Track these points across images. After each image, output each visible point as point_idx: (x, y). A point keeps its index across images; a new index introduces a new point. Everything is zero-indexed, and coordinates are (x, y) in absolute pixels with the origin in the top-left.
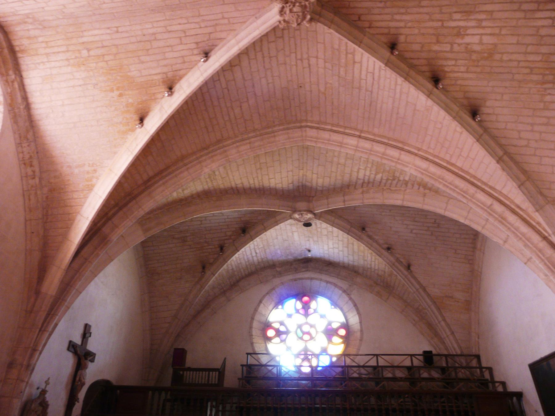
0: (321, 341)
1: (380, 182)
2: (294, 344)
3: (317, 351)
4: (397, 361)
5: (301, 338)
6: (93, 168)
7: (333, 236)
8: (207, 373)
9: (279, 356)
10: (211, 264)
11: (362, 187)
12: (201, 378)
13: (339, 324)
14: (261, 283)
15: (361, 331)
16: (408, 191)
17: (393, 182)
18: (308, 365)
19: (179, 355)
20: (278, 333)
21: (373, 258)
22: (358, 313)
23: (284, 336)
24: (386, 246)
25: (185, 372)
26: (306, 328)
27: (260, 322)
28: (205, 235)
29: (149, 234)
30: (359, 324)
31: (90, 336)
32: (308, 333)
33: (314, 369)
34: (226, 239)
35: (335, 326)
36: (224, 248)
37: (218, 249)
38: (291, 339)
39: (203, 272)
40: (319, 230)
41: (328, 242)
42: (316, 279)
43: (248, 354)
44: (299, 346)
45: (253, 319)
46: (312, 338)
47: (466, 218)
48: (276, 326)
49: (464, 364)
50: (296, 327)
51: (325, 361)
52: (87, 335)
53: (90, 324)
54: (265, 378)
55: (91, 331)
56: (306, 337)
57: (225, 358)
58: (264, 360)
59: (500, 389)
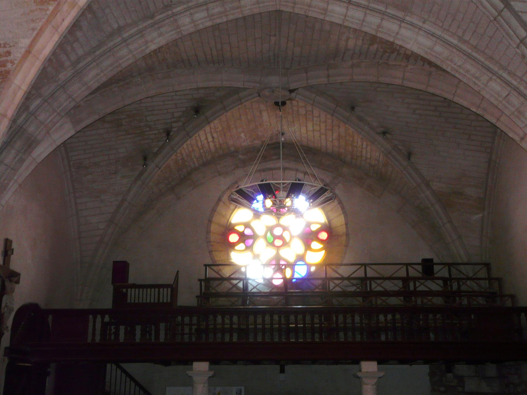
0: (297, 247)
1: (375, 55)
2: (263, 250)
3: (292, 260)
4: (388, 271)
5: (272, 244)
6: (5, 50)
7: (313, 117)
8: (157, 290)
9: (246, 267)
10: (156, 154)
11: (352, 58)
12: (148, 297)
13: (319, 226)
14: (220, 175)
15: (347, 235)
16: (410, 67)
17: (390, 52)
18: (281, 276)
19: (120, 270)
20: (243, 237)
21: (365, 143)
22: (343, 213)
23: (250, 241)
24: (382, 129)
25: (129, 290)
26: (278, 231)
27: (219, 225)
28: (146, 116)
29: (79, 128)
30: (344, 226)
31: (12, 253)
32: (281, 237)
33: (287, 282)
34: (174, 122)
35: (314, 228)
36: (171, 133)
37: (164, 135)
38: (260, 245)
39: (145, 164)
40: (295, 108)
41: (307, 127)
42: (291, 169)
43: (206, 266)
44: (270, 253)
45: (210, 221)
46: (285, 244)
47: (479, 107)
48: (240, 228)
49: (471, 275)
50: (265, 230)
51: (301, 272)
52: (9, 253)
53: (10, 238)
54: (228, 295)
55: (13, 247)
56: (278, 243)
57: (178, 271)
58: (226, 272)
59: (509, 303)
